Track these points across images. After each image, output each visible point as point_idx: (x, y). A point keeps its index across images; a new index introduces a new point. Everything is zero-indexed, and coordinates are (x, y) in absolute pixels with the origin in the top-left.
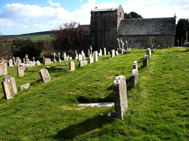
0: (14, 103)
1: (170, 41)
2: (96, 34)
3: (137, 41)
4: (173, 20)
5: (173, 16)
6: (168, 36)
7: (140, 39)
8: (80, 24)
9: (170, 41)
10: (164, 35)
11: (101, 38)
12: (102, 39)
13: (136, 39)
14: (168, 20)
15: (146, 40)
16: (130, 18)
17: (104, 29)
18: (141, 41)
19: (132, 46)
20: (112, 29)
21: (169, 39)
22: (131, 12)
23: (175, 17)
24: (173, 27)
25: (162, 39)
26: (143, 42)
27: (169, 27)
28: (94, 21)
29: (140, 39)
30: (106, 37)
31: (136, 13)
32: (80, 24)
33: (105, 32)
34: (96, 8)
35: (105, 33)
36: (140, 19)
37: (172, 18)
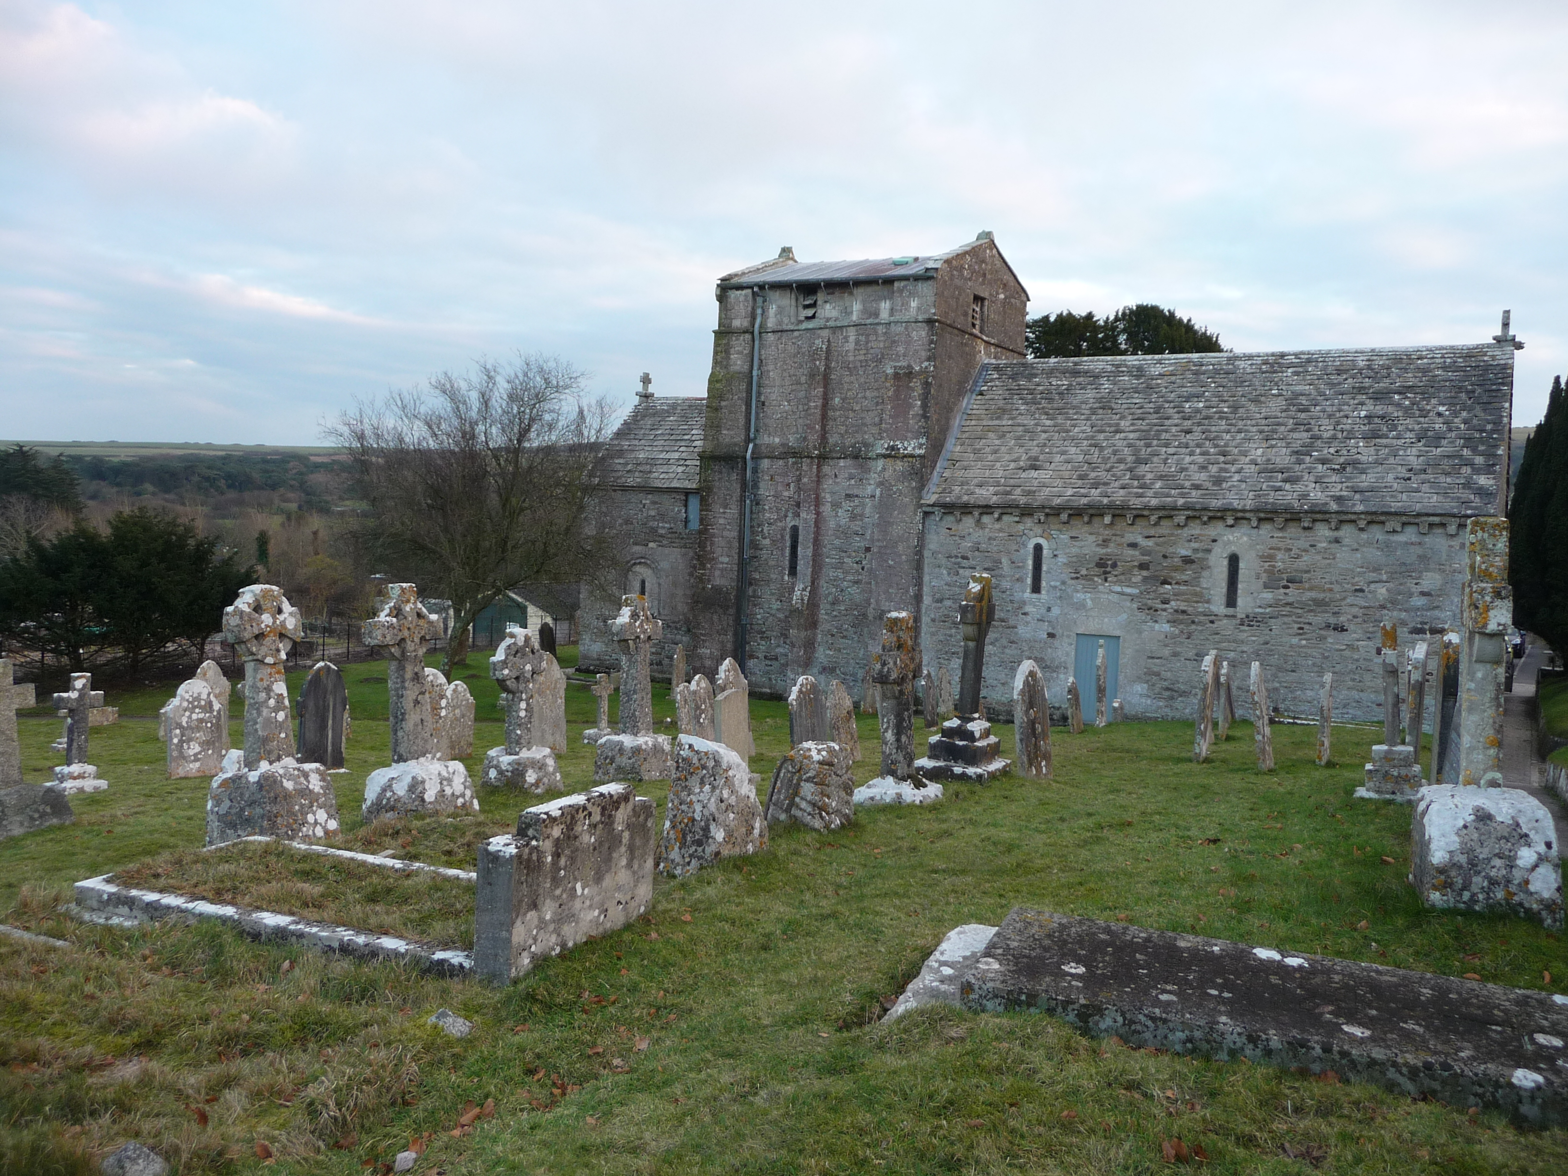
0: (989, 720)
1: (1431, 580)
2: (748, 487)
3: (1105, 567)
4: (1046, 318)
5: (1484, 334)
6: (1410, 535)
7: (1133, 545)
8: (660, 390)
9: (1431, 580)
10: (1376, 518)
11: (790, 522)
12: (795, 530)
13: (1088, 542)
14: (1425, 371)
15: (1188, 561)
16: (1115, 350)
17: (813, 438)
18: (1143, 566)
19: (1056, 611)
20: (881, 447)
21: (1422, 558)
22: (1132, 302)
23: (1507, 341)
24: (1469, 442)
25: (1344, 557)
26: (1154, 578)
27: (1437, 439)
28: (738, 362)
29: (1133, 545)
30: (826, 509)
31: (1178, 315)
32: (651, 389)
33: (826, 469)
34: (786, 252)
35: (819, 478)
36: (1210, 357)
37: (1471, 354)
